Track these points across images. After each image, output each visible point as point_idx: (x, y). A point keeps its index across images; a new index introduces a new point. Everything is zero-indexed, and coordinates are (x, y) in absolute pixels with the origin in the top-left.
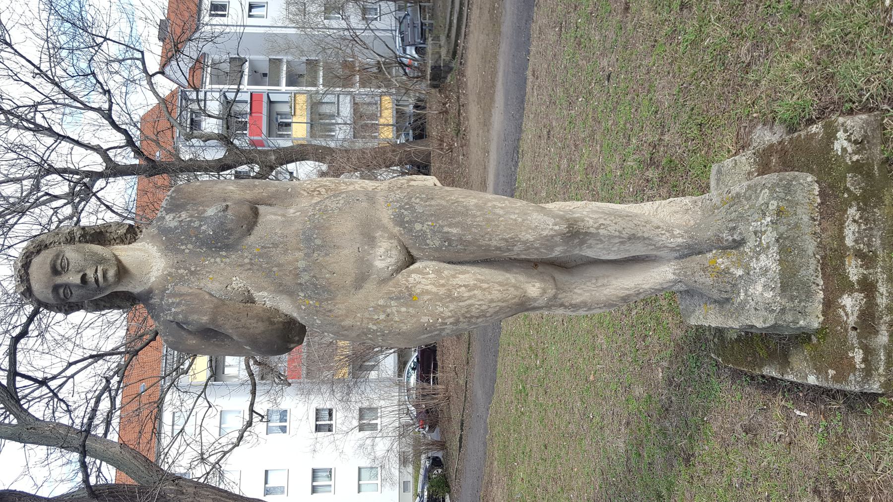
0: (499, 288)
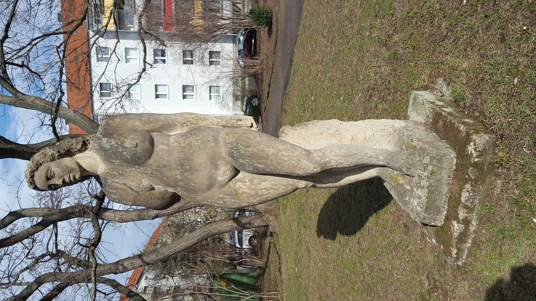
0: (283, 188)
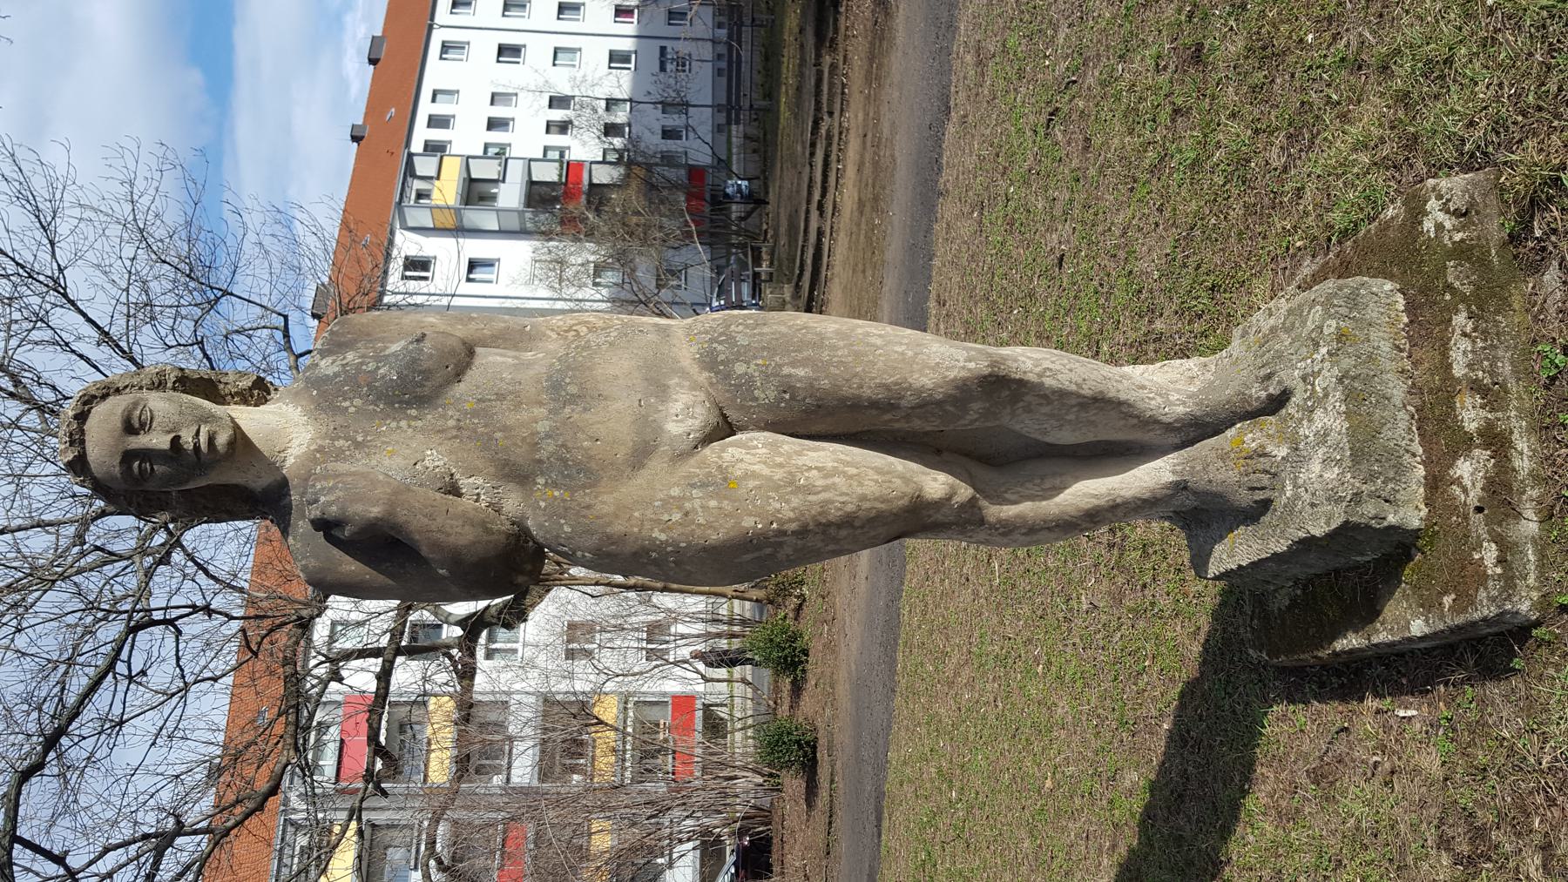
0: (876, 477)
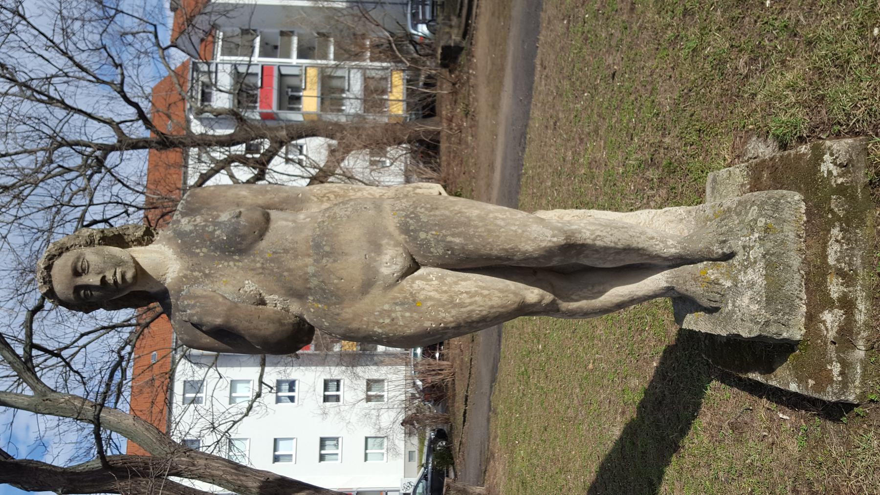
0: (499, 295)
